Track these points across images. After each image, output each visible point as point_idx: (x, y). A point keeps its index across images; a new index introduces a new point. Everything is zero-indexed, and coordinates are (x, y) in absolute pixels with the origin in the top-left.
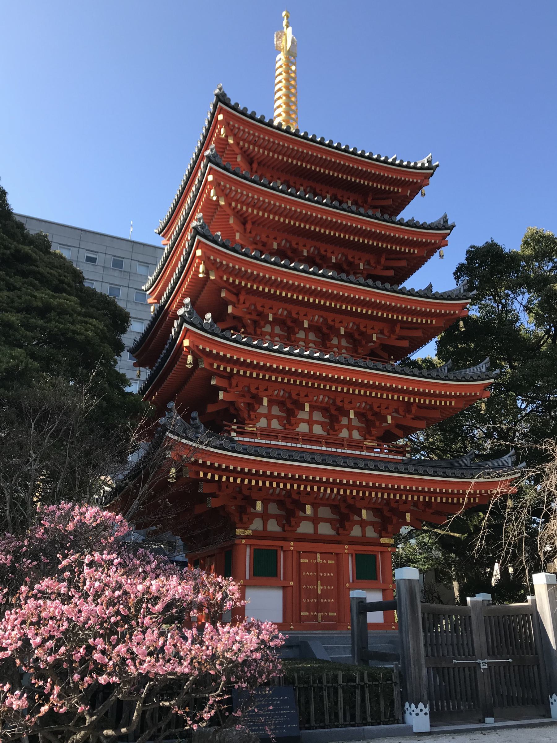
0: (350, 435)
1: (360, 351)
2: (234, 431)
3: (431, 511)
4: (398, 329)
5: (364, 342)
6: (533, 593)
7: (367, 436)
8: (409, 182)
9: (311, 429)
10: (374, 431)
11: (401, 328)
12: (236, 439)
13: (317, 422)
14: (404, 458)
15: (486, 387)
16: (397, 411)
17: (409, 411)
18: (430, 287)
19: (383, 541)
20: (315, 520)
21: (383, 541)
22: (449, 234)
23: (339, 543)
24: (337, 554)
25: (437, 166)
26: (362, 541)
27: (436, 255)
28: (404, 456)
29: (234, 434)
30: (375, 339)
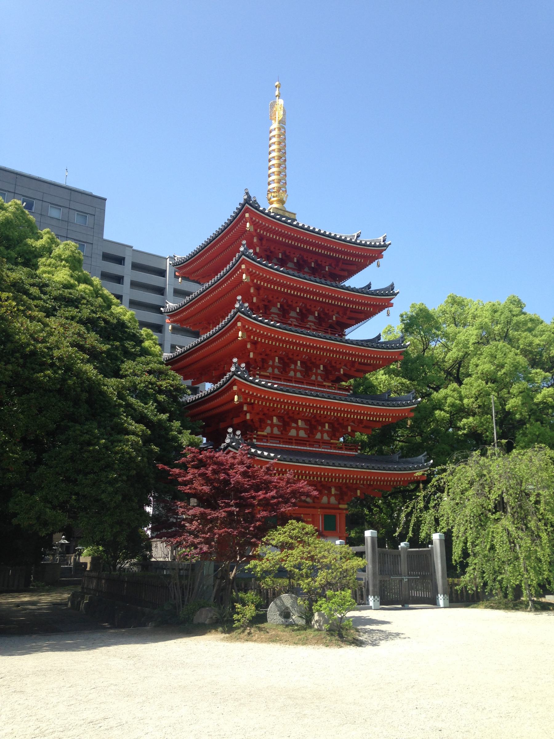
0: (322, 437)
1: (323, 325)
2: (255, 438)
3: (362, 426)
4: (348, 312)
5: (326, 320)
6: (432, 544)
7: (326, 380)
8: (366, 255)
9: (298, 434)
10: (331, 377)
11: (343, 263)
12: (256, 443)
13: (302, 429)
14: (356, 453)
15: (412, 410)
16: (345, 365)
17: (353, 366)
18: (369, 286)
19: (341, 506)
20: (298, 429)
21: (341, 506)
22: (385, 250)
23: (314, 507)
24: (313, 515)
25: (390, 244)
26: (328, 506)
27: (375, 263)
28: (349, 392)
29: (254, 440)
30: (327, 269)
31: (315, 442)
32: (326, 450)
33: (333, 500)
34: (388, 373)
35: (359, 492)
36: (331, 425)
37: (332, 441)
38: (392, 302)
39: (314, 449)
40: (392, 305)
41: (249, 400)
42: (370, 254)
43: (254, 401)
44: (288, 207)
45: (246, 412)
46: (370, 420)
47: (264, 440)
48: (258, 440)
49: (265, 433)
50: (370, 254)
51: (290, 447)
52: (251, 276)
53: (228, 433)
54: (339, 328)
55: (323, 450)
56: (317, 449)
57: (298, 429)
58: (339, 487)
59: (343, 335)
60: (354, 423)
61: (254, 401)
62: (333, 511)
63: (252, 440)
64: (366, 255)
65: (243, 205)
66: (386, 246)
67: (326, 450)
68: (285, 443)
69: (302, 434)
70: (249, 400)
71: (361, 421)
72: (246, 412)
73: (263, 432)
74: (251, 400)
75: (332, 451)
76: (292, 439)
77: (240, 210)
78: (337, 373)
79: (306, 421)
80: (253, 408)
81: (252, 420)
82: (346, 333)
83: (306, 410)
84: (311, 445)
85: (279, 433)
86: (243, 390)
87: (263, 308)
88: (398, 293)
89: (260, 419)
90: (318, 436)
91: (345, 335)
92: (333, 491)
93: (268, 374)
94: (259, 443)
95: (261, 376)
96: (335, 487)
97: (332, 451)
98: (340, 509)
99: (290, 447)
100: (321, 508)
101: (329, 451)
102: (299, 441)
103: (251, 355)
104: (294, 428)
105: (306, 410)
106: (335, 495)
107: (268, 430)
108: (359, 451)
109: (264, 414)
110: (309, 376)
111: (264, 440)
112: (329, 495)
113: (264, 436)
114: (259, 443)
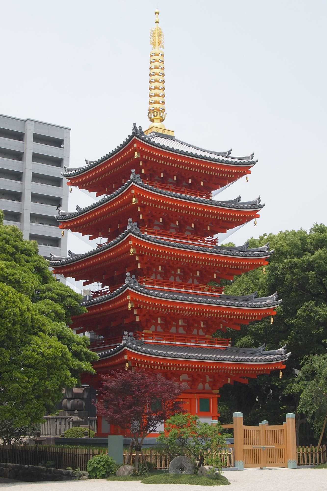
2: (143, 337)
8: (234, 170)
12: (144, 341)
18: (239, 198)
19: (214, 391)
21: (214, 391)
23: (191, 393)
24: (190, 399)
29: (143, 338)
31: (191, 338)
32: (201, 345)
33: (207, 386)
34: (265, 328)
35: (229, 379)
36: (206, 323)
37: (206, 336)
38: (258, 213)
39: (192, 344)
40: (258, 216)
41: (140, 253)
42: (238, 170)
43: (145, 253)
44: (168, 125)
45: (136, 315)
46: (232, 268)
47: (150, 338)
48: (146, 338)
49: (150, 332)
50: (238, 170)
51: (172, 343)
52: (140, 152)
53: (127, 276)
54: (207, 191)
55: (199, 345)
56: (194, 344)
57: (178, 326)
58: (206, 322)
59: (209, 197)
60: (219, 271)
61: (145, 253)
62: (207, 395)
63: (142, 284)
64: (234, 170)
65: (131, 137)
66: (254, 163)
67: (201, 345)
68: (168, 339)
69: (181, 330)
70: (140, 253)
71: (231, 320)
72: (138, 262)
73: (148, 330)
74: (142, 252)
75: (206, 345)
76: (173, 336)
77: (128, 141)
78: (204, 230)
79: (185, 319)
80: (143, 259)
81: (140, 321)
82: (212, 195)
83: (183, 260)
84: (189, 341)
85: (162, 330)
86: (137, 244)
87: (150, 177)
88: (264, 205)
89: (148, 267)
90: (195, 332)
91: (211, 196)
92: (208, 379)
93: (151, 332)
94: (146, 341)
95: (149, 233)
96: (209, 375)
97: (206, 345)
98: (213, 394)
99: (172, 343)
100: (197, 393)
101: (204, 345)
102: (180, 338)
103: (141, 217)
104: (174, 325)
105: (183, 260)
106: (210, 382)
107: (153, 328)
108: (230, 345)
109: (150, 316)
110: (187, 280)
111: (150, 338)
112: (204, 382)
113: (150, 334)
114: (146, 341)
